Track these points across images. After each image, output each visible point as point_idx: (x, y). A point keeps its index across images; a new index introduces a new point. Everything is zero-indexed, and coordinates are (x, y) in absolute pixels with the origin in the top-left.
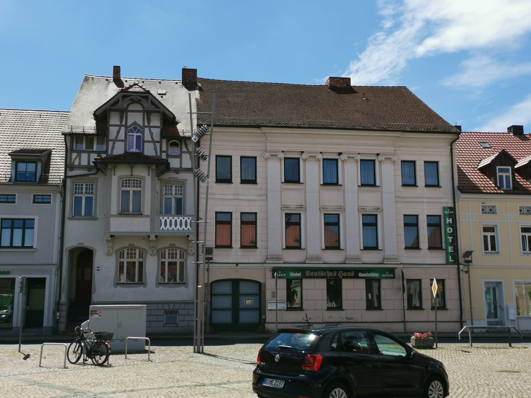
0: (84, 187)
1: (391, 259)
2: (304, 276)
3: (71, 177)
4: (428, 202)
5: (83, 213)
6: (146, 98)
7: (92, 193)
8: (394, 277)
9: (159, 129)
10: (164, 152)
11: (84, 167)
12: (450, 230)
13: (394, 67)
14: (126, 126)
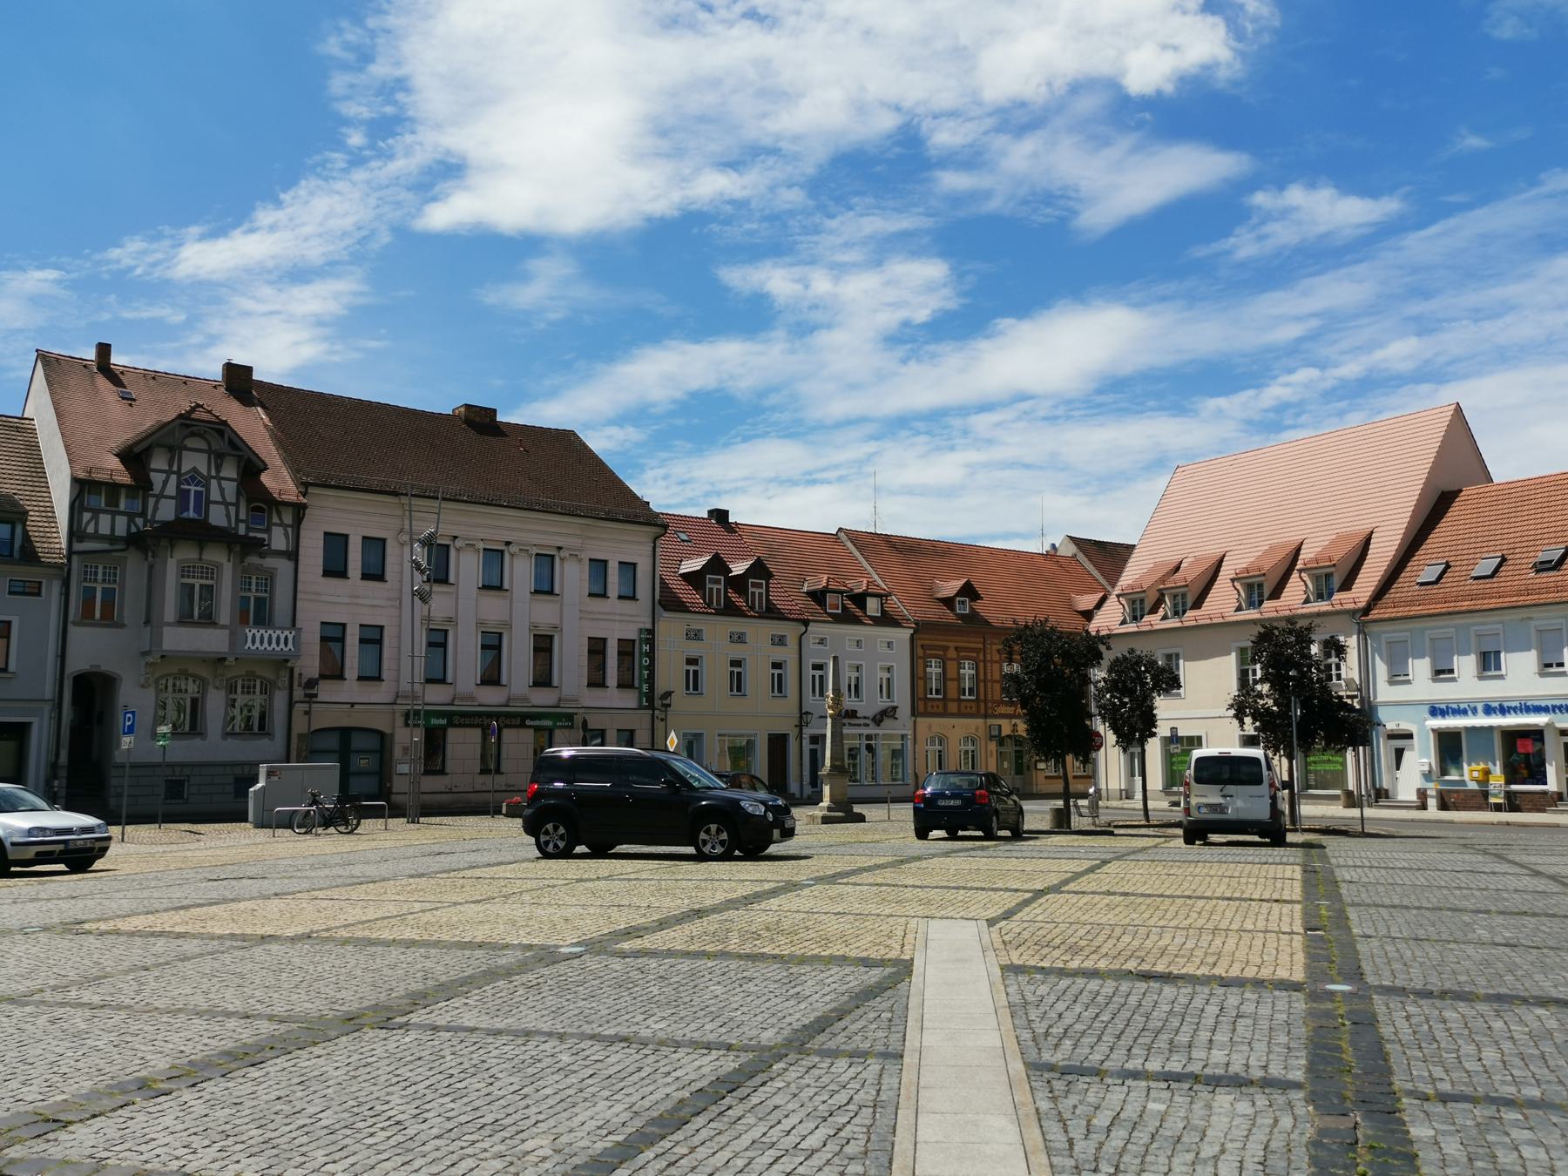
0: (100, 570)
1: (572, 700)
2: (451, 724)
3: (79, 553)
4: (621, 621)
5: (98, 615)
6: (221, 433)
7: (115, 581)
8: (572, 727)
9: (235, 483)
10: (242, 521)
11: (103, 538)
12: (646, 661)
13: (365, 238)
14: (178, 473)
